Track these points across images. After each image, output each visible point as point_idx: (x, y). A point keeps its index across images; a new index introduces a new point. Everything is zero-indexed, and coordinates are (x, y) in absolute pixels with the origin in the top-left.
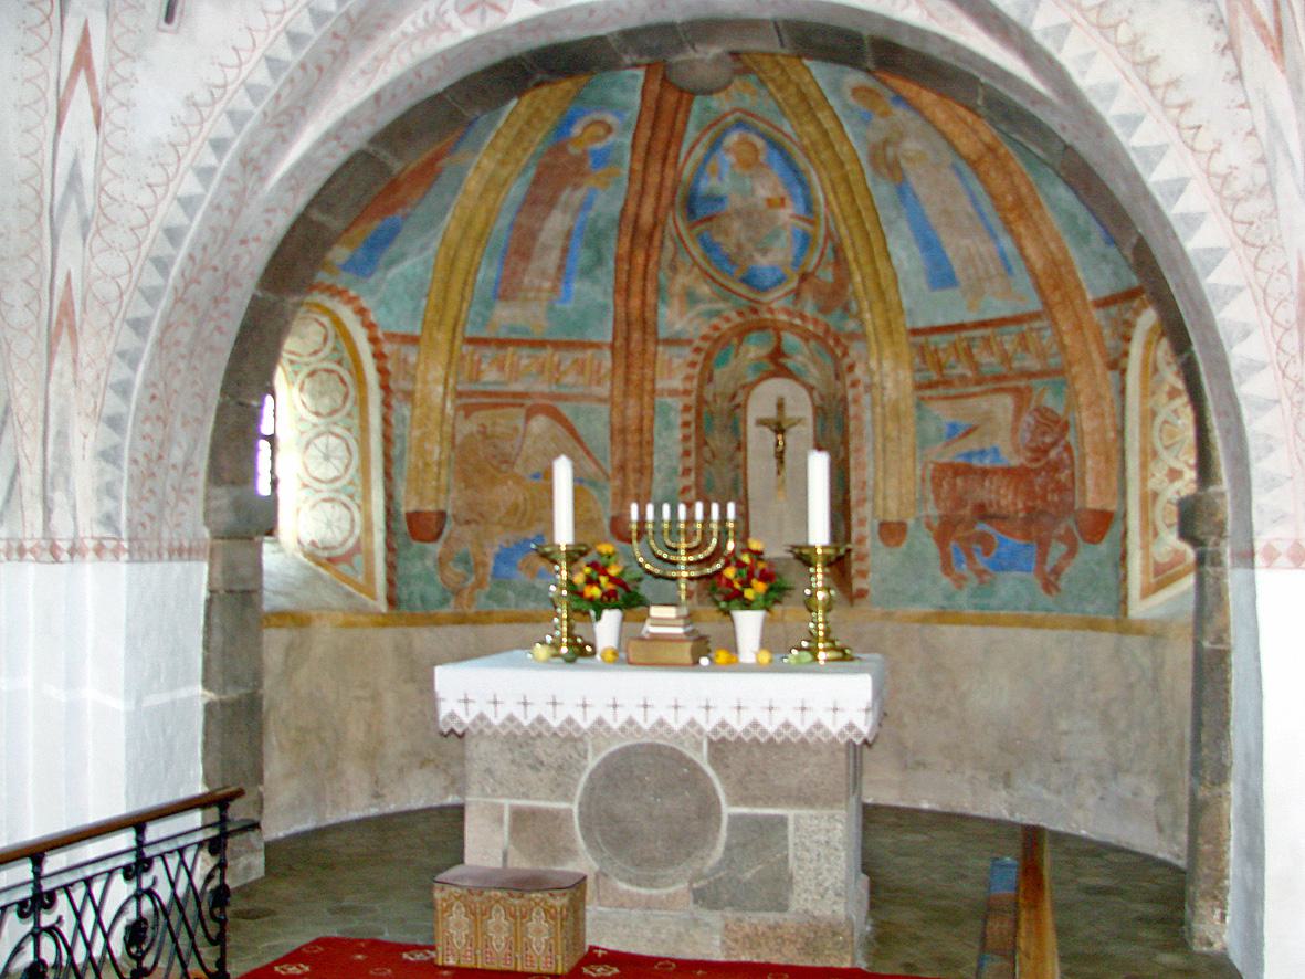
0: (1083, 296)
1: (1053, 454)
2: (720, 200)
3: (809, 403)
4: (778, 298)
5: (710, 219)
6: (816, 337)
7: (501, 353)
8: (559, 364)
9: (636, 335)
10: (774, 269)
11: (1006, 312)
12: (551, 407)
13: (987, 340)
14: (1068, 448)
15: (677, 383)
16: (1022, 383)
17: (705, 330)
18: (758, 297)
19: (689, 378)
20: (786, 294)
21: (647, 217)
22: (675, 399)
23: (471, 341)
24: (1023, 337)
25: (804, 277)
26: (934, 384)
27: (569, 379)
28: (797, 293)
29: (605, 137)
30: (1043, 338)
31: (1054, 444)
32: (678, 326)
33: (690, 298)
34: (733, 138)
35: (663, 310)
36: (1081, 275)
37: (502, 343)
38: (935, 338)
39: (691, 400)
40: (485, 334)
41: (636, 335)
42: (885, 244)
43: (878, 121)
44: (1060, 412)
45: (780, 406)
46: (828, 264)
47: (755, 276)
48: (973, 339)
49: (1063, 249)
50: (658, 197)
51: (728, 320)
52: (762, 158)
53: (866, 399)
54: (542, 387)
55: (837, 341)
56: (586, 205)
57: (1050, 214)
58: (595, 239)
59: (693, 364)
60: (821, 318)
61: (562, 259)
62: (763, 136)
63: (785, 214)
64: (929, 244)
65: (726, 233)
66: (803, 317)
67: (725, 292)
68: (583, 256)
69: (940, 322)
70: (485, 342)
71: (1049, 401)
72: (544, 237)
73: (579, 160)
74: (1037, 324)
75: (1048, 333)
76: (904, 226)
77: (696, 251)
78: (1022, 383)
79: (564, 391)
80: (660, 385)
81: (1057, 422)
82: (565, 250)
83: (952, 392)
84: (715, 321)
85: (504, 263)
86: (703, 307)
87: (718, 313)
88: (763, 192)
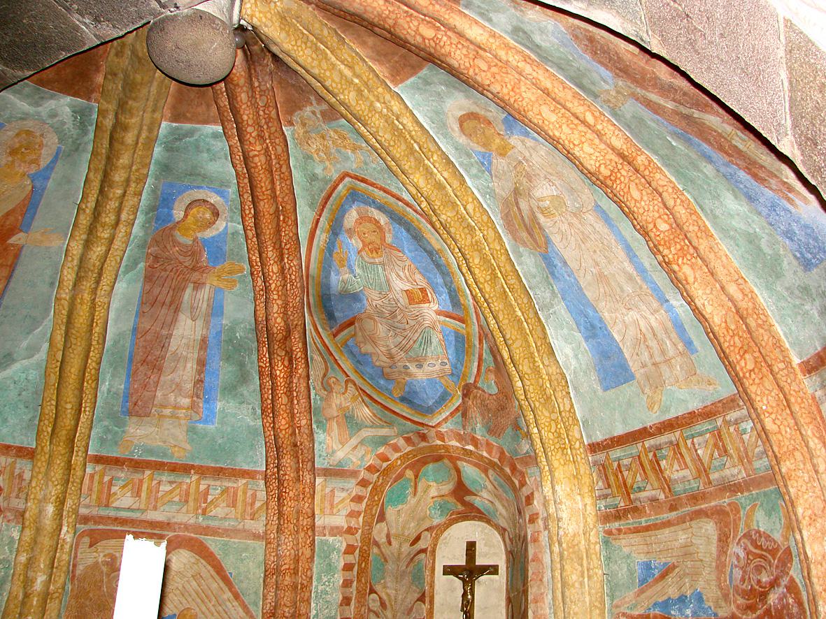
0: (789, 363)
1: (773, 598)
2: (356, 297)
3: (503, 547)
4: (446, 420)
5: (351, 323)
6: (492, 464)
7: (137, 476)
8: (207, 493)
9: (289, 460)
10: (432, 382)
11: (694, 405)
12: (197, 540)
13: (676, 446)
14: (792, 588)
15: (340, 520)
16: (725, 501)
17: (370, 460)
18: (425, 421)
19: (352, 514)
20: (452, 414)
21: (278, 322)
22: (338, 538)
23: (98, 460)
24: (718, 434)
25: (467, 391)
26: (621, 513)
27: (219, 511)
28: (463, 412)
29: (210, 224)
30: (744, 432)
31: (774, 584)
32: (340, 455)
33: (350, 422)
34: (352, 216)
35: (320, 436)
36: (778, 329)
37: (138, 465)
38: (616, 453)
39: (356, 540)
40: (115, 453)
41: (287, 461)
42: (545, 336)
43: (500, 163)
44: (777, 536)
45: (471, 547)
46: (488, 370)
47: (415, 392)
48: (659, 448)
49: (750, 296)
50: (285, 296)
51: (396, 448)
52: (389, 239)
53: (544, 537)
54: (185, 517)
55: (514, 469)
56: (215, 310)
57: (724, 247)
58: (234, 351)
59: (358, 499)
60: (492, 440)
61: (200, 372)
62: (381, 208)
63: (430, 311)
64: (593, 330)
65: (373, 340)
66: (475, 442)
67: (387, 414)
68: (223, 371)
69: (619, 430)
70: (117, 462)
71: (761, 522)
72: (174, 345)
73: (193, 252)
74: (732, 416)
75: (748, 425)
76: (561, 308)
77: (346, 364)
78: (725, 501)
79: (212, 523)
80: (318, 522)
81: (773, 552)
82: (202, 363)
83: (643, 522)
84: (382, 450)
85: (132, 374)
86: (365, 433)
87: (384, 441)
88: (400, 285)
